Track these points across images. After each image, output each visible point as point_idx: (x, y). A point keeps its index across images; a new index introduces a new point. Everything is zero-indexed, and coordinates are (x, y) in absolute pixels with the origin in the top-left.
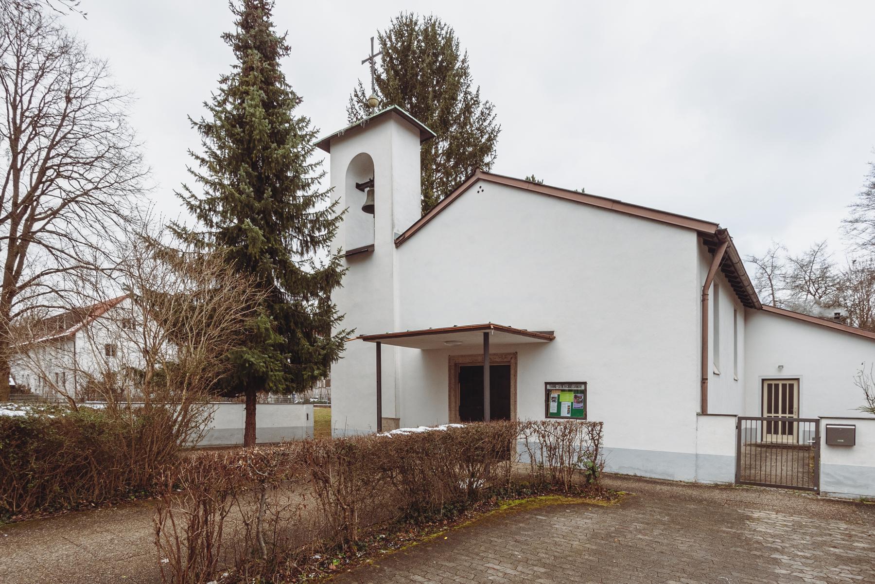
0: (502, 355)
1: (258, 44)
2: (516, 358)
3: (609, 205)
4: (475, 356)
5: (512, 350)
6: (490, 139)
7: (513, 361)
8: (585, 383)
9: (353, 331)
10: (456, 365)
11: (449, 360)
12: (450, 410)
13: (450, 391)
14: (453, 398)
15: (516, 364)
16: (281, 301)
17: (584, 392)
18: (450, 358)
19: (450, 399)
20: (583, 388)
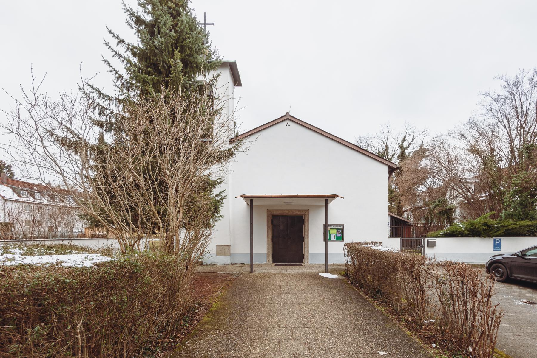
0: (300, 210)
1: (170, 59)
2: (308, 212)
3: (355, 148)
4: (284, 210)
5: (306, 209)
6: (222, 199)
7: (306, 214)
8: (343, 225)
9: (404, 140)
10: (271, 214)
11: (267, 213)
12: (268, 238)
13: (268, 229)
14: (269, 233)
15: (308, 215)
16: (413, 215)
17: (342, 230)
18: (268, 211)
19: (267, 233)
20: (342, 227)
